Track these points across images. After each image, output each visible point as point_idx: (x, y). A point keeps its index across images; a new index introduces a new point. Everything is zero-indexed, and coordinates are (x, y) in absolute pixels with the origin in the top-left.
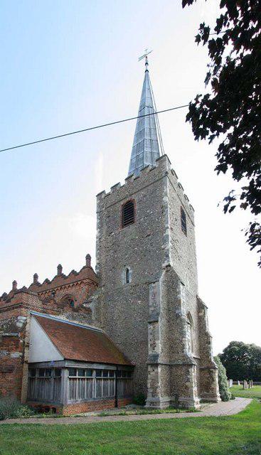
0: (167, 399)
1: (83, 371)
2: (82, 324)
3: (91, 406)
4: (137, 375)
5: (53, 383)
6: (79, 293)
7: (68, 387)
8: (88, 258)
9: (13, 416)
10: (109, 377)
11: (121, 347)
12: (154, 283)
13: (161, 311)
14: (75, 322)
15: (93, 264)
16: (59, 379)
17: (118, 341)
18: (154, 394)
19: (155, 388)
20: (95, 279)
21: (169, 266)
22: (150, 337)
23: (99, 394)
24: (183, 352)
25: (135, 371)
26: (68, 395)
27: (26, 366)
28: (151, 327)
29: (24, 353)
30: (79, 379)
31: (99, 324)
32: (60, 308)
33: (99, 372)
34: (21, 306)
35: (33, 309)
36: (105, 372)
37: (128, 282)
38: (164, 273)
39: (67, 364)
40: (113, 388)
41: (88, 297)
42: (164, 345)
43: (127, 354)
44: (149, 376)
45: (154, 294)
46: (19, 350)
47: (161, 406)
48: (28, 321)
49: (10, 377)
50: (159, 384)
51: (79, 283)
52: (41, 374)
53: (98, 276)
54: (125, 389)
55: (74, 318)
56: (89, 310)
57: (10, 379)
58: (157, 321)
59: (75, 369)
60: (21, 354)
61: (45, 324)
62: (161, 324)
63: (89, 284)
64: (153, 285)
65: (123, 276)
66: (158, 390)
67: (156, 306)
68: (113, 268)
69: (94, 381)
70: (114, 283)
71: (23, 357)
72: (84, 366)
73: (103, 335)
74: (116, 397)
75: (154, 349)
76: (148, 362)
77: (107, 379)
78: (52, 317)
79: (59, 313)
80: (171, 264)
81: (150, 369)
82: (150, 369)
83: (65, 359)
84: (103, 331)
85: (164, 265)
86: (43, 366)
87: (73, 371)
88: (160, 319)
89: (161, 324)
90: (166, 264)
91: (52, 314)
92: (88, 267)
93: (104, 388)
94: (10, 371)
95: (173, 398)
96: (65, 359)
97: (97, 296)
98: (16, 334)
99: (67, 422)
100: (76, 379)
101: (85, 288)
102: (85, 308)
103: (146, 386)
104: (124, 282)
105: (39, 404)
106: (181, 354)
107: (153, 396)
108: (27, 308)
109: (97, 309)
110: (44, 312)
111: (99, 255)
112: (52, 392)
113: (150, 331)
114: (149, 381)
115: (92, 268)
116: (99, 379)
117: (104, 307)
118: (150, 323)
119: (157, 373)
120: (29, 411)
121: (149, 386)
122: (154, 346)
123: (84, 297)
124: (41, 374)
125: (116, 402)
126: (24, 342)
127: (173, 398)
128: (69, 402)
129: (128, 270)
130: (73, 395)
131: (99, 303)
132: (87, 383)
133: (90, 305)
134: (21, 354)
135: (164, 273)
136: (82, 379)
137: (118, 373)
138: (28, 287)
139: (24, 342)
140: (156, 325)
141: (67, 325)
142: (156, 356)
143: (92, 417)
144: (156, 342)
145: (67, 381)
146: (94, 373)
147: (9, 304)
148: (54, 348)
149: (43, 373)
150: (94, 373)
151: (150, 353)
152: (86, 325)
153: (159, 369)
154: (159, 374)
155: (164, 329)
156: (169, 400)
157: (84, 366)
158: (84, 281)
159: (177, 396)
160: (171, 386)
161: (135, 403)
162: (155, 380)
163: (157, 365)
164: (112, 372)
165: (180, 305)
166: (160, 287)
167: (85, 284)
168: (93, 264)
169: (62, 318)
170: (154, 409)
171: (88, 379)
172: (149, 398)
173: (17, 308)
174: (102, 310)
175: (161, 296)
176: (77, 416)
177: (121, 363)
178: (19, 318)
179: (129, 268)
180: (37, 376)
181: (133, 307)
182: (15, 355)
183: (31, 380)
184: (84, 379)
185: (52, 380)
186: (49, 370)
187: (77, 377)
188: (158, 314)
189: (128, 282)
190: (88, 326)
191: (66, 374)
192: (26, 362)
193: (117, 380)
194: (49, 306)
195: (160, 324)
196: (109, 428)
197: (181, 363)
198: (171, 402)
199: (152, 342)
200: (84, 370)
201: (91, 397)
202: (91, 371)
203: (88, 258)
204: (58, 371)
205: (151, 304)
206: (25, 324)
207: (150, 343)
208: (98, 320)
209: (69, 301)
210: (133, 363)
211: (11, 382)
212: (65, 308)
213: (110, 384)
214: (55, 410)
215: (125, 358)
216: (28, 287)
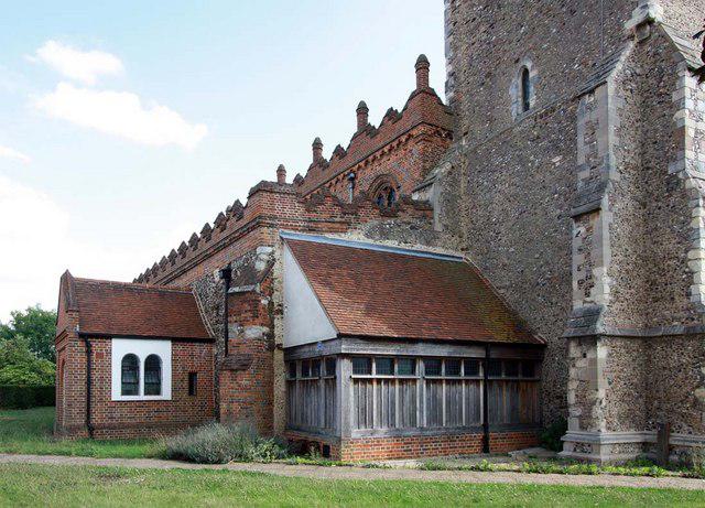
0: (632, 436)
1: (387, 363)
2: (408, 246)
3: (408, 444)
4: (549, 367)
5: (323, 391)
6: (402, 167)
7: (352, 399)
8: (422, 65)
9: (242, 457)
10: (443, 376)
11: (511, 297)
12: (591, 92)
13: (615, 176)
14: (389, 243)
15: (438, 80)
16: (332, 382)
17: (502, 282)
18: (586, 422)
19: (588, 405)
20: (444, 121)
21: (649, 21)
22: (578, 259)
23: (434, 417)
24: (689, 295)
25: (547, 359)
26: (352, 418)
27: (279, 356)
28: (580, 228)
29: (272, 326)
30: (379, 381)
31: (455, 240)
32: (349, 215)
33: (433, 364)
34: (259, 225)
35: (286, 227)
36: (453, 364)
37: (526, 106)
38: (627, 53)
39: (345, 348)
40: (393, 403)
41: (426, 171)
42: (624, 278)
43: (525, 314)
44: (573, 372)
45: (592, 129)
46: (260, 320)
47: (605, 454)
48: (277, 255)
49: (245, 380)
50: (601, 394)
51: (403, 139)
52: (305, 373)
53: (452, 111)
54: (514, 408)
55: (385, 235)
56: (425, 209)
57: (244, 382)
58: (597, 210)
59: (369, 359)
60: (266, 329)
61: (305, 255)
62: (612, 220)
63: (426, 138)
64: (588, 99)
65: (515, 92)
66: (597, 411)
67: (597, 163)
68: (489, 75)
69: (421, 387)
70: (491, 120)
71: (271, 336)
72: (391, 350)
73: (465, 268)
74: (485, 426)
75: (588, 295)
76: (570, 332)
77: (460, 382)
78: (331, 238)
79: (346, 226)
80: (657, 13)
81: (574, 351)
82: (574, 351)
83: (340, 336)
84: (468, 258)
85: (630, 25)
86: (306, 354)
87: (361, 363)
88: (605, 202)
89: (612, 220)
90: (637, 17)
91: (331, 231)
92: (424, 92)
93: (448, 403)
94: (244, 367)
95: (652, 436)
96: (340, 336)
97: (448, 166)
98: (250, 288)
99: (355, 475)
100: (371, 381)
101: (416, 148)
102: (415, 204)
103: (562, 397)
104: (516, 109)
105: (303, 436)
106: (681, 302)
107: (583, 427)
108: (272, 226)
109: (450, 201)
110: (311, 230)
111: (452, 47)
112: (323, 410)
113: (577, 243)
114: (573, 385)
115: (432, 93)
116: (434, 381)
117: (471, 192)
118: (577, 218)
119: (594, 362)
120: (276, 450)
121: (572, 398)
122: (588, 284)
123: (416, 176)
124: (305, 373)
125: (485, 441)
126: (271, 303)
127: (652, 436)
128: (355, 433)
129: (526, 72)
130: (364, 418)
131: (454, 183)
132: (401, 391)
133: (430, 195)
134: (266, 329)
135: (627, 53)
136: (387, 381)
137: (491, 366)
138: (303, 174)
139: (271, 303)
140: (594, 222)
141: (368, 254)
142: (593, 314)
143: (407, 468)
144: (595, 272)
145: (347, 386)
146: (420, 366)
147: (243, 222)
148: (320, 309)
149: (310, 367)
150: (420, 366)
151: (578, 305)
152: (418, 247)
153: (602, 352)
154: (601, 366)
155: (624, 230)
156: (640, 439)
157: (391, 350)
158: (414, 132)
159: (665, 431)
160: (649, 401)
161: (542, 443)
162: (589, 383)
163: (592, 340)
164: (472, 366)
165: (681, 146)
166: (613, 99)
167: (418, 140)
168: (438, 80)
169: (356, 238)
170: (585, 458)
171: (402, 381)
172: (573, 432)
173: (253, 228)
174: (464, 203)
175: (612, 128)
176: (368, 466)
177: (500, 338)
178: (258, 250)
179: (529, 65)
180: (299, 376)
181: (539, 177)
182: (254, 332)
183: (290, 384)
184: (393, 381)
185: (322, 384)
186: (315, 363)
187: (374, 376)
188: (601, 188)
189: (526, 106)
190: (424, 248)
191: (345, 369)
192: (279, 347)
193: (487, 383)
194: (322, 213)
195: (606, 217)
196: (529, 490)
197: (679, 329)
198: (645, 445)
199: (582, 275)
200: (392, 360)
201: (413, 423)
202: (413, 360)
203: (422, 65)
204: (331, 362)
205: (581, 160)
206: (271, 264)
207: (577, 276)
208: (453, 230)
209: (385, 201)
210: (540, 337)
211: (246, 388)
212: (361, 213)
213: (467, 394)
214: (326, 452)
215: (519, 326)
216: (303, 174)
